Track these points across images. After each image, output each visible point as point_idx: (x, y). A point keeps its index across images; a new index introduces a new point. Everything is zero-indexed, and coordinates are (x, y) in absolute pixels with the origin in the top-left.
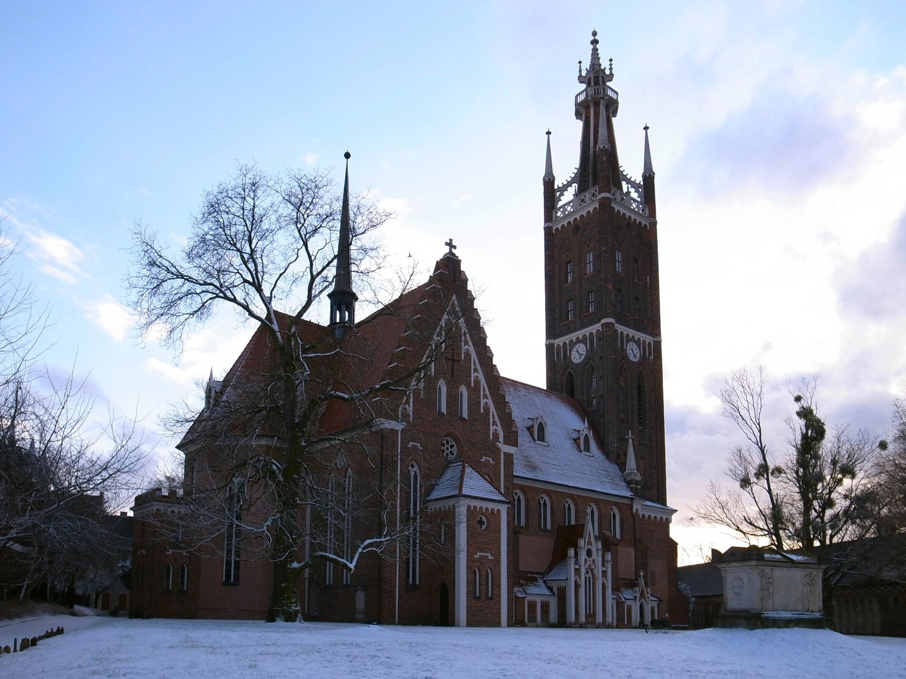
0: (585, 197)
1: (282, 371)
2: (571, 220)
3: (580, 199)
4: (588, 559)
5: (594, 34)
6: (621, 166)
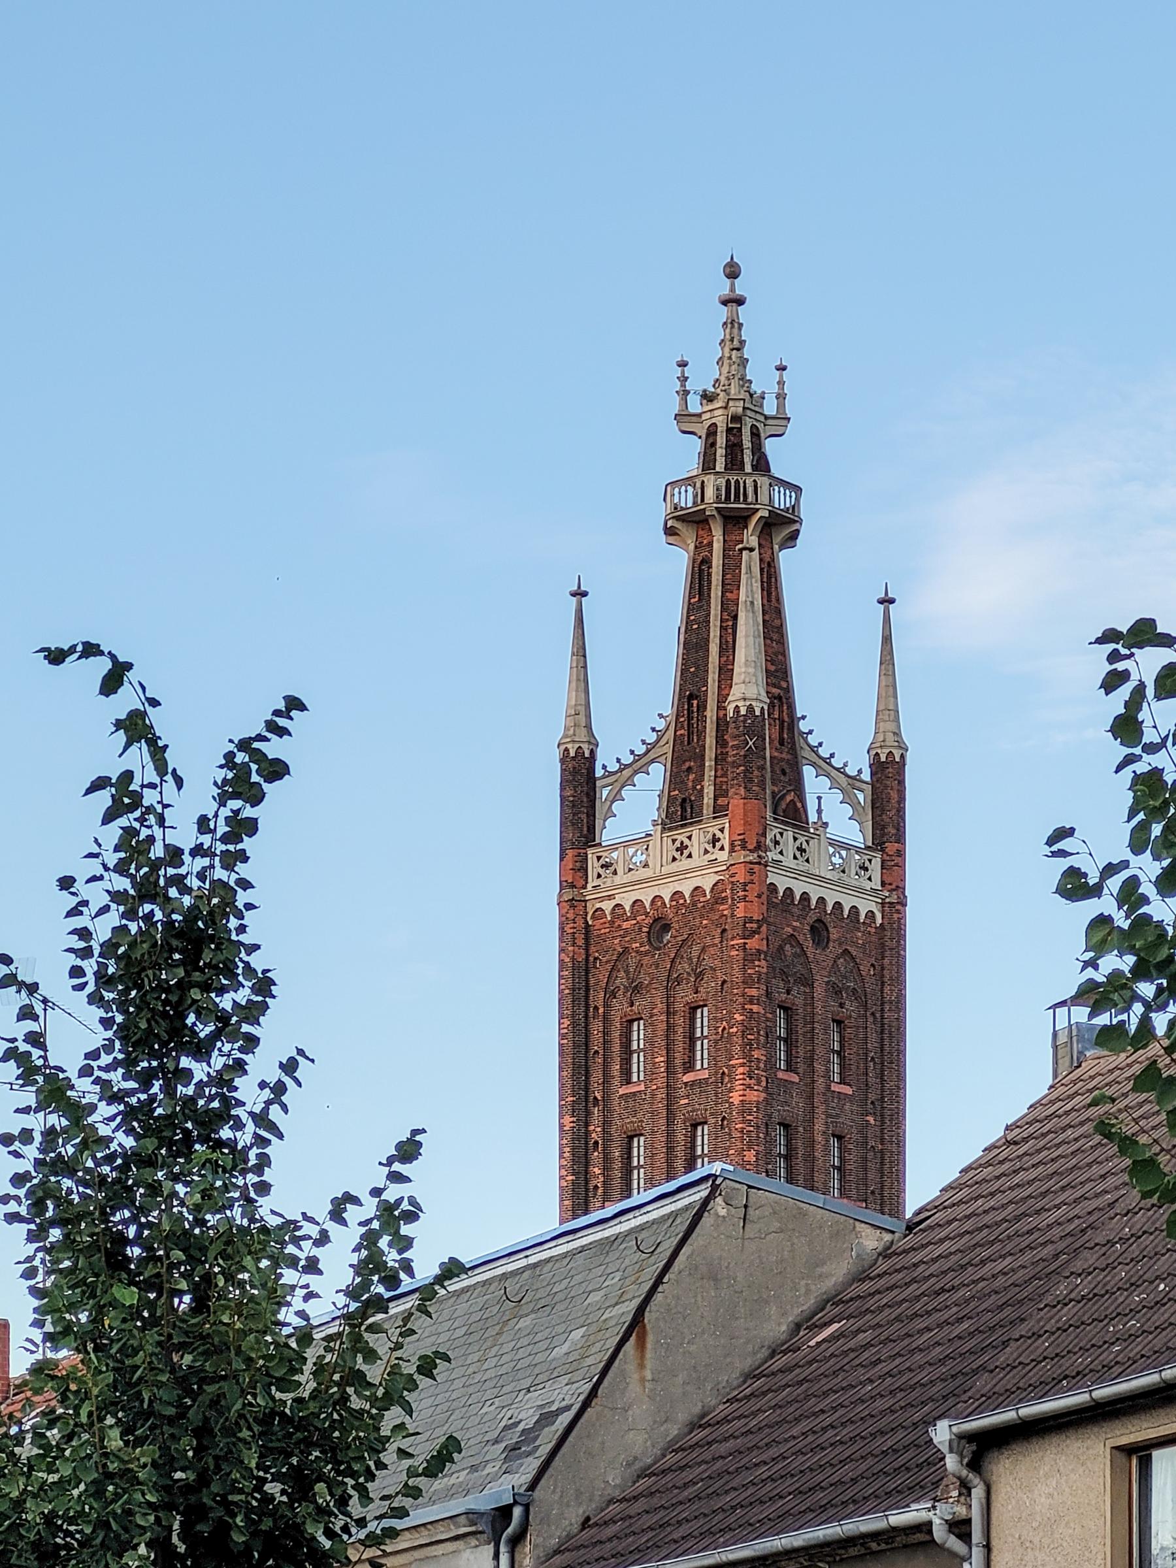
0: (690, 838)
1: (132, 1231)
2: (686, 888)
3: (674, 841)
4: (776, 605)
5: (732, 271)
6: (804, 717)
